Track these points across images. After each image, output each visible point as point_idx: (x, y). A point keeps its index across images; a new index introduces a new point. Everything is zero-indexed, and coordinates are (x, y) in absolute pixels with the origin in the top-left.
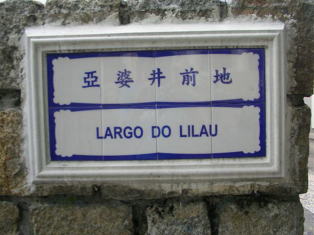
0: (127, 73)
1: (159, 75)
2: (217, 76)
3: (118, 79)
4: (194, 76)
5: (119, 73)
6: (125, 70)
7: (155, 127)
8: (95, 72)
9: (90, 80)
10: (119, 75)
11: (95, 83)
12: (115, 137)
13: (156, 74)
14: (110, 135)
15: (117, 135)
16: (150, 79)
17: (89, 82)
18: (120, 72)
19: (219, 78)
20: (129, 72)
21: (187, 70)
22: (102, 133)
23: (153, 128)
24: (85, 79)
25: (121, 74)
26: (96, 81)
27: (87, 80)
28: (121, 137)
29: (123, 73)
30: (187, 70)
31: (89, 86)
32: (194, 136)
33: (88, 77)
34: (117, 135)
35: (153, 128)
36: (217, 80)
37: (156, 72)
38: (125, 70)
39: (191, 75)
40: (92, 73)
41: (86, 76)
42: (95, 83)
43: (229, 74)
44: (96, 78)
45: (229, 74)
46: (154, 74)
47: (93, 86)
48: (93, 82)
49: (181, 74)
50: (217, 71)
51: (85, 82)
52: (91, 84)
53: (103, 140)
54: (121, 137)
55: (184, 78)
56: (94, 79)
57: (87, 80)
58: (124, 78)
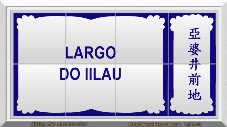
0: (196, 45)
1: (196, 63)
2: (190, 94)
3: (190, 49)
4: (198, 78)
5: (191, 45)
6: (195, 43)
7: (64, 69)
8: (198, 29)
9: (194, 34)
10: (191, 46)
11: (197, 37)
12: (86, 57)
13: (194, 61)
14: (81, 54)
15: (88, 55)
16: (190, 65)
17: (193, 35)
18: (191, 45)
19: (192, 96)
20: (198, 45)
21: (193, 74)
22: (72, 53)
23: (62, 69)
24: (190, 33)
25: (192, 46)
26: (198, 34)
27: (192, 34)
28: (92, 57)
29: (193, 45)
30: (193, 74)
31: (193, 38)
32: (95, 79)
33: (193, 32)
34: (88, 55)
35: (62, 69)
36: (191, 97)
37: (195, 60)
38: (195, 43)
39: (196, 78)
40: (196, 29)
41: (191, 31)
42: (197, 37)
43: (199, 93)
44: (198, 32)
45: (199, 93)
46: (193, 62)
47: (196, 38)
48: (196, 35)
49: (189, 77)
50: (191, 91)
51: (191, 35)
52: (194, 37)
53: (101, 80)
54: (92, 57)
55: (191, 80)
56: (197, 33)
57: (192, 34)
58: (194, 48)
